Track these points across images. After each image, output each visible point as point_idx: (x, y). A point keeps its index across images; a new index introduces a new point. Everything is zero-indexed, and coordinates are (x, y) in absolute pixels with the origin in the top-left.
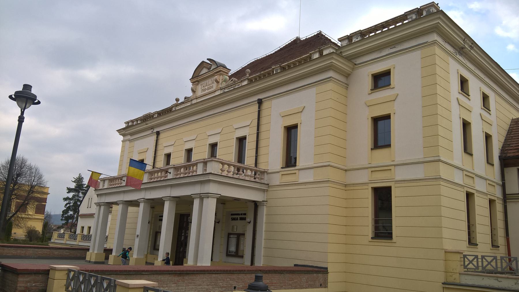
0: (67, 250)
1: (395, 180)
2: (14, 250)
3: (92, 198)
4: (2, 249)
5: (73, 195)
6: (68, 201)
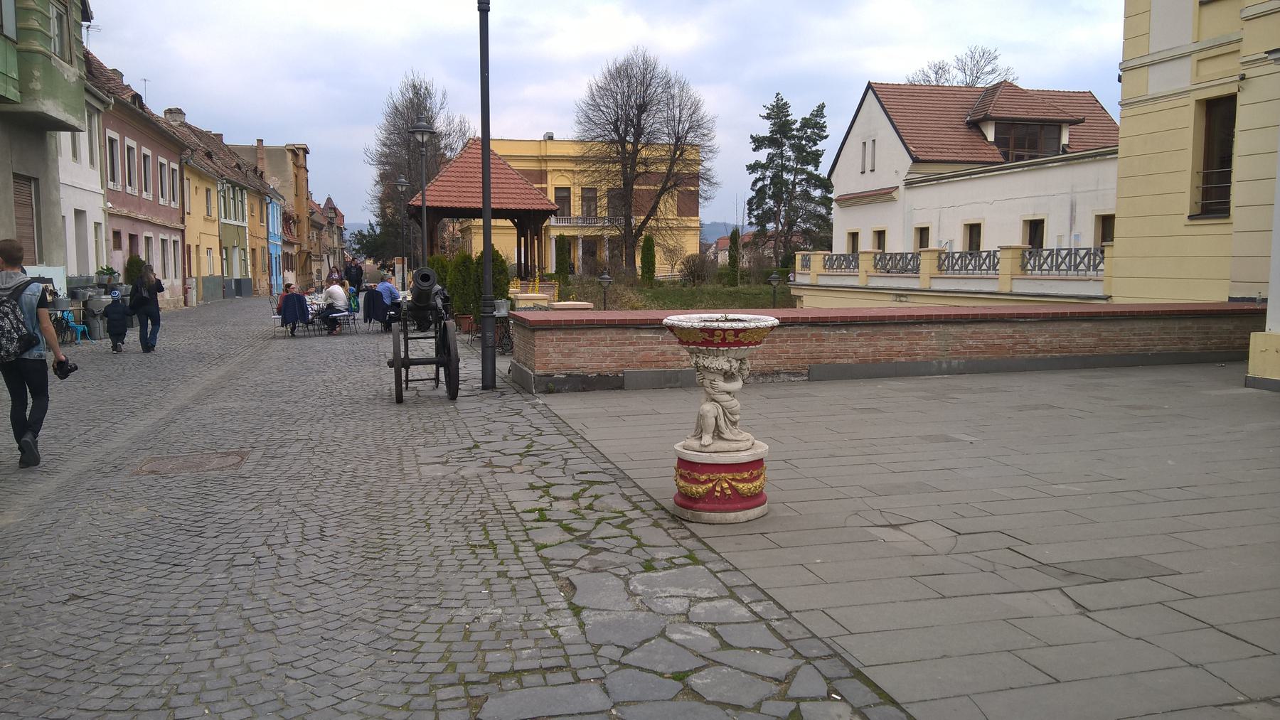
0: (1085, 325)
2: (861, 338)
3: (874, 141)
4: (813, 335)
5: (768, 156)
6: (760, 173)
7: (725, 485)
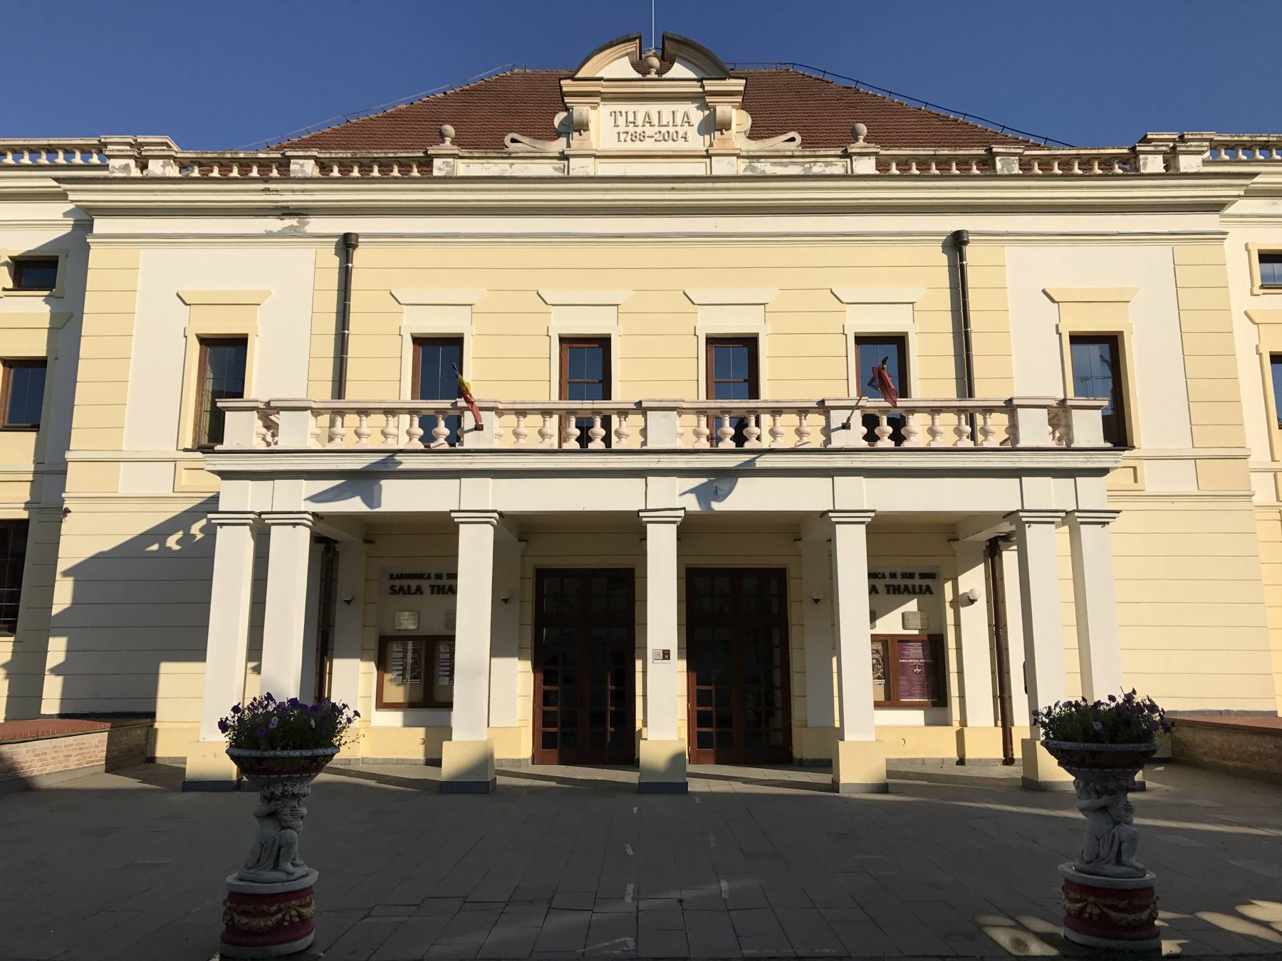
1: (40, 506)
7: (294, 913)
